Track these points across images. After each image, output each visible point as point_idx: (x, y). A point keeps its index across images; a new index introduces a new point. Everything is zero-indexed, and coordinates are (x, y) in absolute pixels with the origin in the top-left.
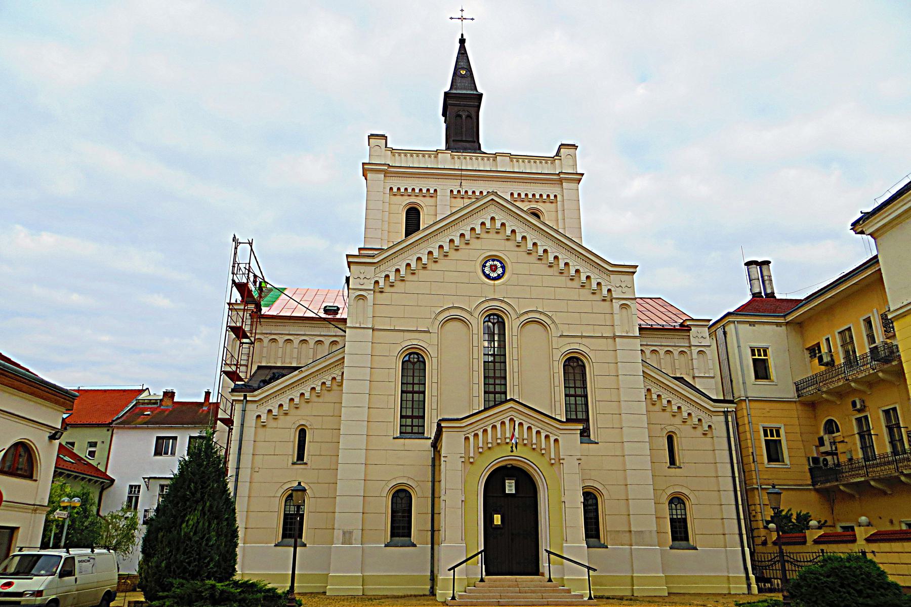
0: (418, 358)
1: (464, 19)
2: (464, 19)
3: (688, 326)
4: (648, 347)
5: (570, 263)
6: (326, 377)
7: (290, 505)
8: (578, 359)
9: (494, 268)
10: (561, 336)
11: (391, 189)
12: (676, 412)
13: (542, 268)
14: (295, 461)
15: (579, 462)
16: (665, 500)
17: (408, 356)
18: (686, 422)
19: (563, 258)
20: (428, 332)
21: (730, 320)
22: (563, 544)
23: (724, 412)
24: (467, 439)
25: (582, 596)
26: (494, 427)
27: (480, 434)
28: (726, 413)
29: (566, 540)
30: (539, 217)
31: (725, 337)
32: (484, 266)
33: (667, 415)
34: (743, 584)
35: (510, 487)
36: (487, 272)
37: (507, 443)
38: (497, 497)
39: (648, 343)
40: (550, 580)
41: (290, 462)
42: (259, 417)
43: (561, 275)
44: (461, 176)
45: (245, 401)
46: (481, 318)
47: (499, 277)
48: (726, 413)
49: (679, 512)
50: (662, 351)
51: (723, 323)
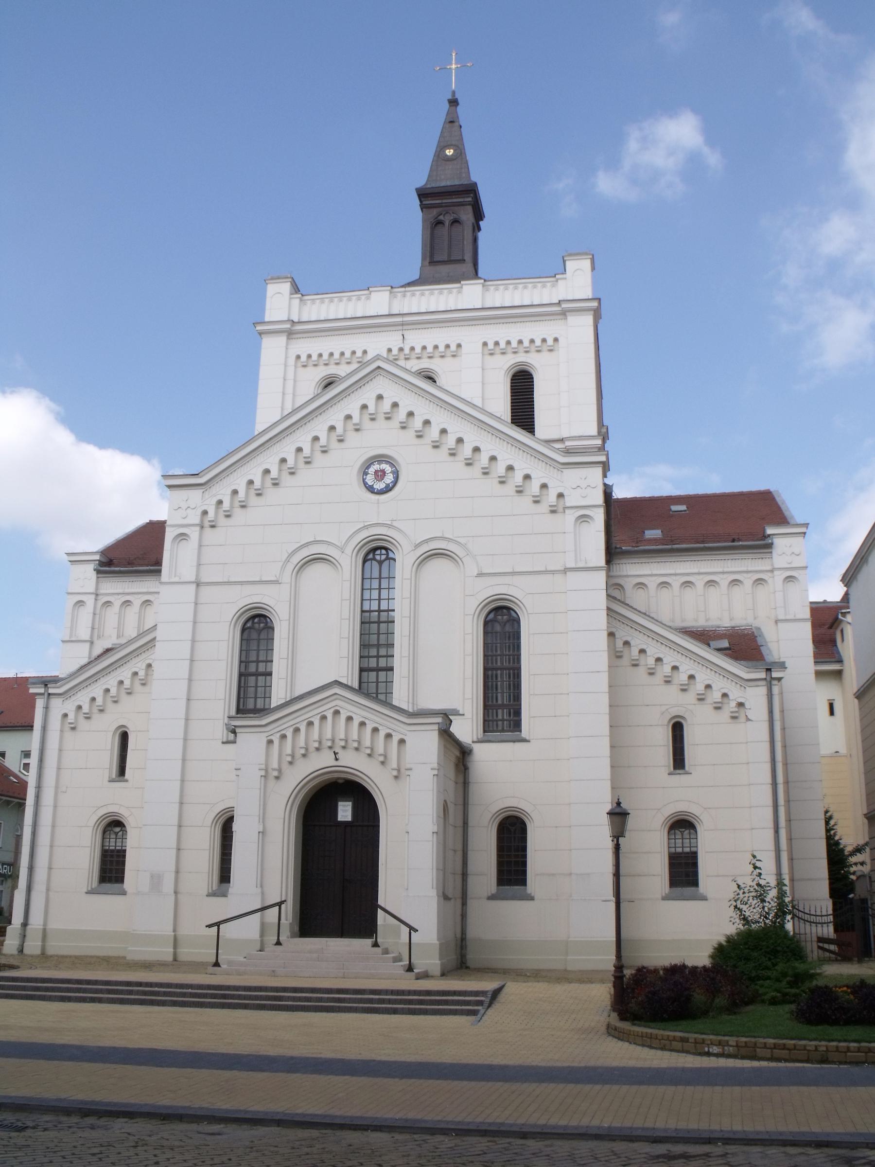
7: (110, 838)
9: (380, 475)
10: (480, 575)
11: (298, 357)
13: (457, 467)
14: (114, 776)
15: (238, 772)
20: (276, 582)
24: (270, 742)
33: (674, 689)
35: (345, 812)
36: (370, 483)
38: (368, 826)
42: (65, 715)
45: (46, 694)
47: (388, 489)
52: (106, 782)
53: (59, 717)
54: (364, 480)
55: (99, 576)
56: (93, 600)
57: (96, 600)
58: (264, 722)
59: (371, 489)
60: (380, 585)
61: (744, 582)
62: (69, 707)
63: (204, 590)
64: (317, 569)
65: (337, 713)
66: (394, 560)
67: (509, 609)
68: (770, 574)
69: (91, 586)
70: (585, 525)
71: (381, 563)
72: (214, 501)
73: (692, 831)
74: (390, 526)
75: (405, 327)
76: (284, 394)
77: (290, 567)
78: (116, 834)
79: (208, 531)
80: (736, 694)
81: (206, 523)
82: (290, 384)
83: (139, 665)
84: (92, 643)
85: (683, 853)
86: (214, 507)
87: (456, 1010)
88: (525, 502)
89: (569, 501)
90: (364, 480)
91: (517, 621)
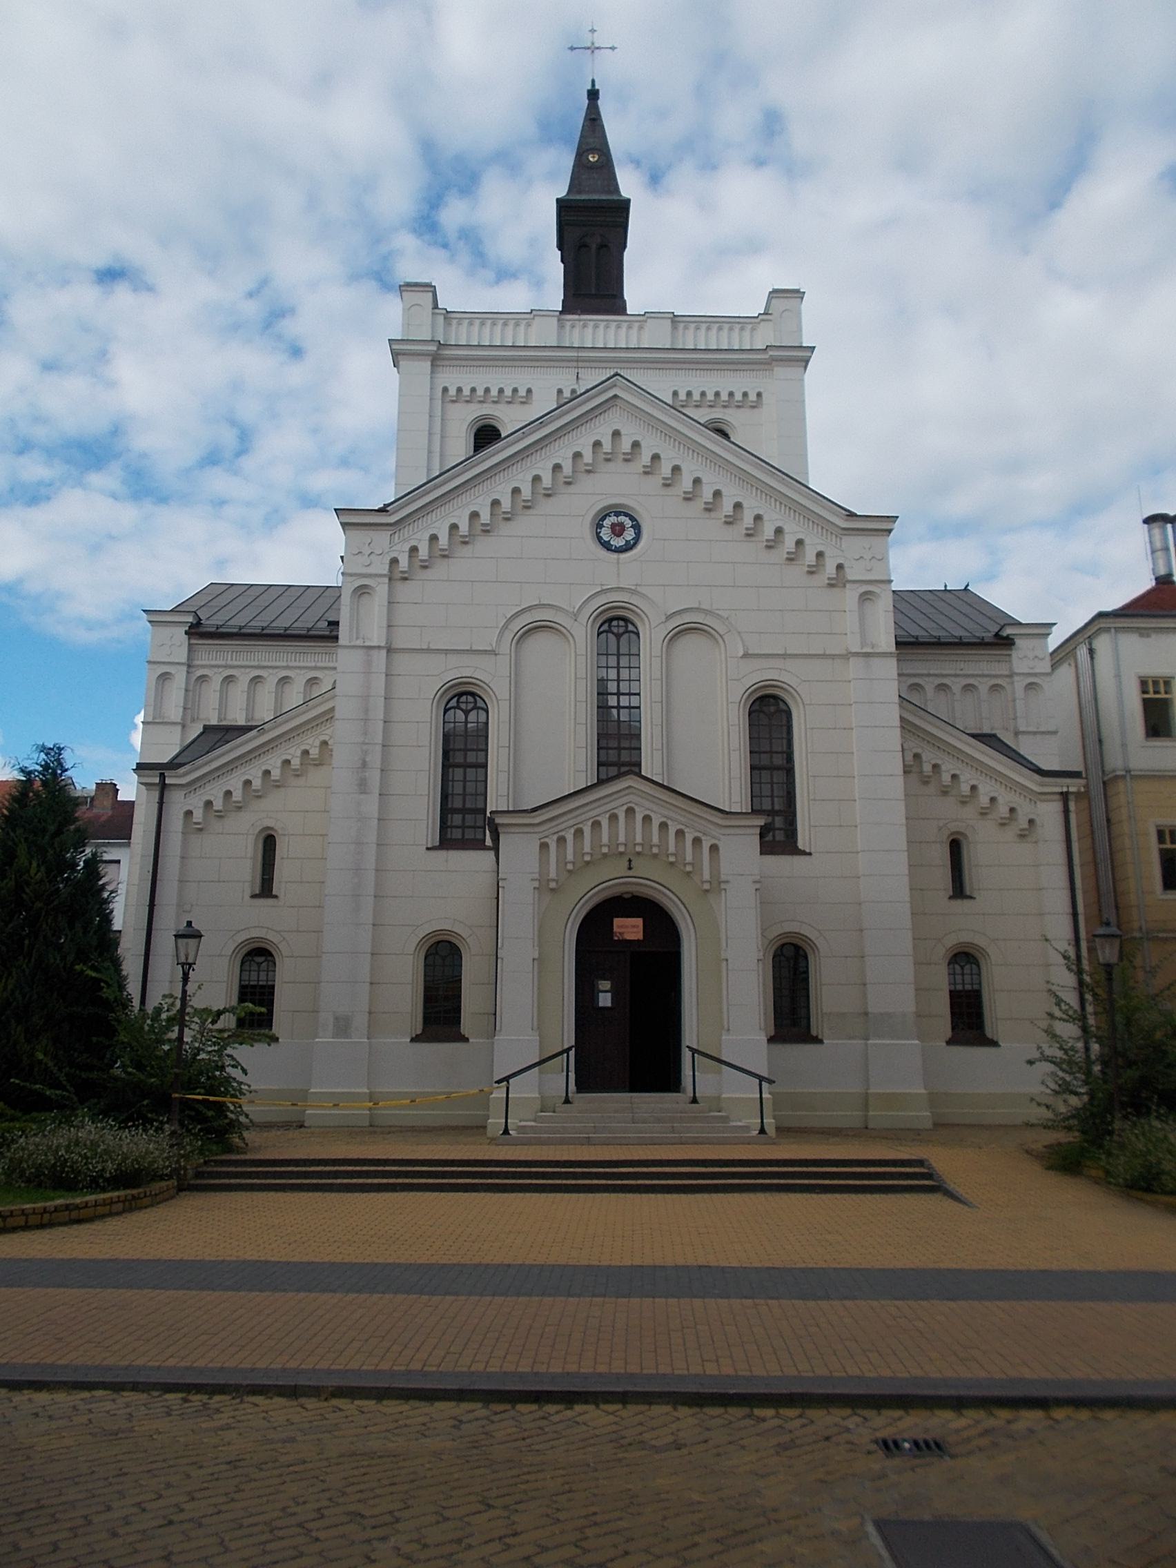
0: (475, 702)
1: (589, 48)
2: (589, 48)
3: (1007, 638)
4: (931, 679)
5: (785, 527)
6: (310, 741)
8: (775, 697)
9: (618, 530)
11: (445, 390)
12: (966, 796)
16: (940, 955)
17: (456, 699)
18: (986, 814)
19: (752, 506)
20: (493, 653)
21: (1102, 626)
22: (721, 1035)
23: (1062, 793)
24: (544, 846)
25: (747, 1128)
26: (596, 825)
27: (570, 837)
28: (1065, 796)
29: (728, 1030)
30: (725, 435)
31: (1092, 658)
32: (600, 526)
34: (499, 1118)
36: (606, 538)
37: (621, 853)
39: (931, 672)
40: (694, 1100)
41: (248, 893)
43: (748, 538)
44: (577, 361)
46: (592, 626)
47: (628, 547)
48: (1065, 796)
49: (968, 978)
50: (956, 685)
51: (1089, 634)
52: (247, 897)
53: (181, 816)
54: (598, 534)
55: (193, 641)
56: (185, 673)
57: (188, 672)
58: (537, 821)
59: (607, 546)
60: (618, 663)
61: (927, 687)
62: (195, 802)
63: (398, 658)
64: (540, 642)
65: (630, 811)
66: (638, 634)
67: (775, 697)
68: (1007, 680)
69: (182, 656)
70: (287, 686)
71: (618, 636)
72: (407, 547)
73: (456, 957)
74: (633, 592)
75: (580, 364)
76: (430, 434)
77: (509, 636)
78: (259, 964)
79: (399, 586)
80: (1025, 811)
81: (396, 576)
82: (438, 420)
83: (292, 751)
84: (184, 726)
85: (964, 991)
86: (407, 555)
87: (380, 1184)
88: (796, 573)
89: (851, 574)
90: (598, 534)
91: (789, 714)
